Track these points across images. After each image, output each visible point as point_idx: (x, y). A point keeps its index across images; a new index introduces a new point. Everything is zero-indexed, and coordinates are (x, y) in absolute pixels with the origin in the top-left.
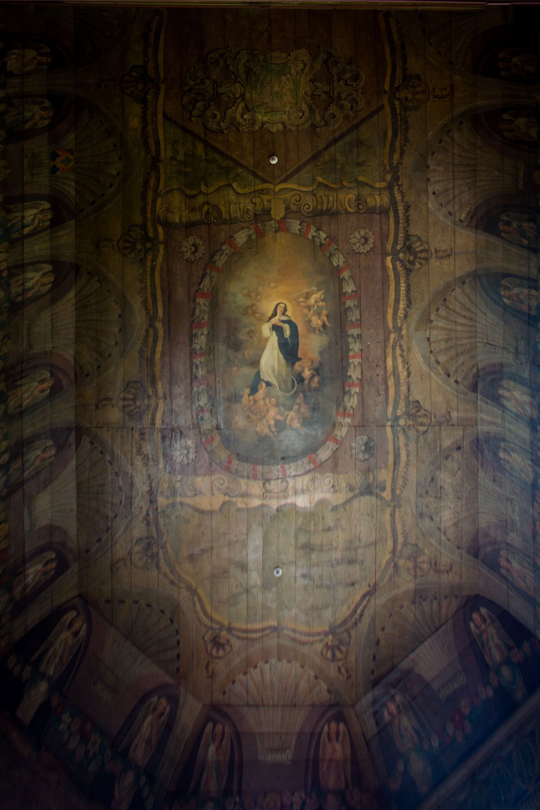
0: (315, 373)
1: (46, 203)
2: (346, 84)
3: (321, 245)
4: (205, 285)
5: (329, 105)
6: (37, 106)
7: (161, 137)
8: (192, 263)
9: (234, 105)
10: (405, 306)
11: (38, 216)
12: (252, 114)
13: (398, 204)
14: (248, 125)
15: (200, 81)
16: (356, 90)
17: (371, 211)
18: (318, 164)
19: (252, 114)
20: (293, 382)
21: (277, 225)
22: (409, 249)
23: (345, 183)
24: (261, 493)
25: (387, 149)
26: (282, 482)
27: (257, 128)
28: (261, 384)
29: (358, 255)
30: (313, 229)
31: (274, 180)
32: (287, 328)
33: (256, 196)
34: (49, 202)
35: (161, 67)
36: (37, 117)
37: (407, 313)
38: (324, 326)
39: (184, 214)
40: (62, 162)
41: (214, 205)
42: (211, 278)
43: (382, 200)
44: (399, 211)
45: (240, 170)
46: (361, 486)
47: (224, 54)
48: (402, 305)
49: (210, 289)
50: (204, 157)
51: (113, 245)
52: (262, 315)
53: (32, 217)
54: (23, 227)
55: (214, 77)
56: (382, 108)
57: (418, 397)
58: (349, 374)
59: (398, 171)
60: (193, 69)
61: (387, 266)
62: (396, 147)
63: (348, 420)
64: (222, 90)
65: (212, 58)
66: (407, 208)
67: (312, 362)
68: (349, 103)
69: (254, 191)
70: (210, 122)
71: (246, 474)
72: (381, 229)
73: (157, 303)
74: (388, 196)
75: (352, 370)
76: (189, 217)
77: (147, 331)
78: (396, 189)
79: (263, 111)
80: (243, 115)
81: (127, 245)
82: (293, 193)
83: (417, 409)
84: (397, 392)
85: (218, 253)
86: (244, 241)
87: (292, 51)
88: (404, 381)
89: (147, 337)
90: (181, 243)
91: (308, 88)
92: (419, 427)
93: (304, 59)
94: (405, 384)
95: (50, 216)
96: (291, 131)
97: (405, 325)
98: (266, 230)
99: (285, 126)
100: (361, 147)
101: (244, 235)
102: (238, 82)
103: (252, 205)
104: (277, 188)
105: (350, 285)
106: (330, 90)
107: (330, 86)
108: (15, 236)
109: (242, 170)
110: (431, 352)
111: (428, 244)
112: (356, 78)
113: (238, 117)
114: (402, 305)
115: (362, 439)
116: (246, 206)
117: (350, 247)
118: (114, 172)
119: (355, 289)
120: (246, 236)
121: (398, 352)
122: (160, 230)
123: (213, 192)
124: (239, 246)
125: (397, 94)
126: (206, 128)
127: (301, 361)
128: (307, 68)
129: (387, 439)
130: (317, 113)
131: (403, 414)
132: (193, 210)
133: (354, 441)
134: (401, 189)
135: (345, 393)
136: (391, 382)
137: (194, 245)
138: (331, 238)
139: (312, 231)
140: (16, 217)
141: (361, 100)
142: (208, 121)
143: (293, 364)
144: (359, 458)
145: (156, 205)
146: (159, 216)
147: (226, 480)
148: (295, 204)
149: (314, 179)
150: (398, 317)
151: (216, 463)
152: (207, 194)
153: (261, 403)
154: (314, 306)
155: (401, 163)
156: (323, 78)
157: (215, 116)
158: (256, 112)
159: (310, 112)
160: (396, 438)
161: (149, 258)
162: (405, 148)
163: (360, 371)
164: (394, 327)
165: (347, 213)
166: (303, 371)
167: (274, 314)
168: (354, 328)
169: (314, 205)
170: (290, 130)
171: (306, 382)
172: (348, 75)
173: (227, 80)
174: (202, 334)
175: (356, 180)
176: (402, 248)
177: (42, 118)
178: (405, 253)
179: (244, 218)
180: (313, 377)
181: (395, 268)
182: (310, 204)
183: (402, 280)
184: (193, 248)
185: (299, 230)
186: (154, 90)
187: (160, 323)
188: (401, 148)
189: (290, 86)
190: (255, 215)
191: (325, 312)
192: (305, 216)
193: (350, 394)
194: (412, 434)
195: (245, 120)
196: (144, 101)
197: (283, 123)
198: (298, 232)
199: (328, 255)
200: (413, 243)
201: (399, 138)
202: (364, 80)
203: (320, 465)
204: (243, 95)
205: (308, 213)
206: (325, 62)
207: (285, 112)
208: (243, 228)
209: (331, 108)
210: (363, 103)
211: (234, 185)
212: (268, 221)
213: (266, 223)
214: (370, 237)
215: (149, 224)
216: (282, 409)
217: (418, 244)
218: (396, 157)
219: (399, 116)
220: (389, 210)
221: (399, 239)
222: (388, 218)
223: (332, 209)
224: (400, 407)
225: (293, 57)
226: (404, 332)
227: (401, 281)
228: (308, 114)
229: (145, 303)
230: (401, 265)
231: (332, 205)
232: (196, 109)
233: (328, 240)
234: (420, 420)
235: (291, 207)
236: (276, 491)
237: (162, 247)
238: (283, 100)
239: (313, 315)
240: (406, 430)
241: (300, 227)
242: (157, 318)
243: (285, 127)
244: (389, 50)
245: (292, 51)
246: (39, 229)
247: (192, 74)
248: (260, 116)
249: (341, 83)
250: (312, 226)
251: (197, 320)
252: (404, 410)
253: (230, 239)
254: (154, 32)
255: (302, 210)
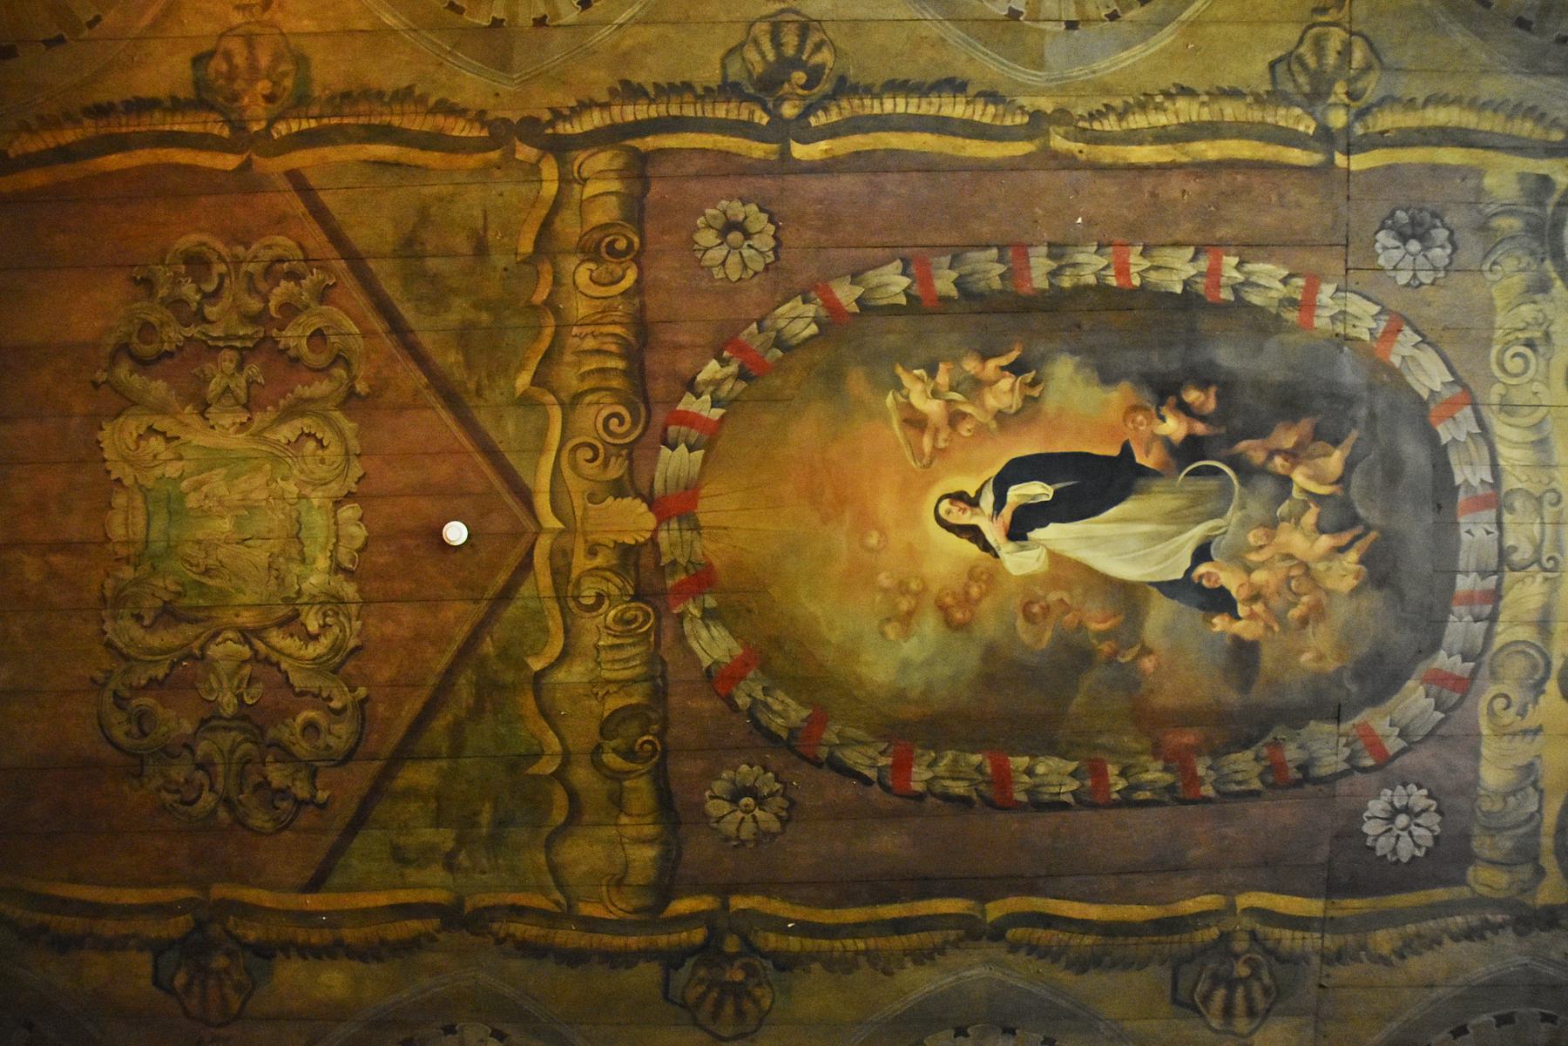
0: (1172, 400)
2: (216, 295)
3: (742, 375)
4: (869, 762)
7: (383, 899)
8: (793, 803)
9: (277, 664)
10: (961, 99)
12: (306, 604)
13: (618, 119)
14: (342, 618)
15: (200, 774)
16: (237, 262)
17: (635, 210)
18: (471, 386)
19: (306, 604)
20: (1196, 473)
21: (674, 525)
22: (768, 87)
23: (541, 296)
24: (1540, 577)
25: (433, 158)
26: (1512, 510)
27: (350, 590)
28: (1201, 577)
29: (783, 255)
30: (688, 404)
31: (522, 534)
32: (1019, 493)
33: (576, 593)
35: (158, 895)
37: (980, 94)
38: (1016, 368)
39: (631, 832)
41: (602, 733)
42: (846, 742)
43: (600, 175)
44: (639, 117)
45: (488, 647)
46: (1532, 253)
47: (115, 693)
48: (956, 109)
49: (883, 746)
50: (444, 764)
52: (972, 575)
55: (187, 727)
56: (296, 179)
57: (1261, 67)
58: (1178, 289)
59: (505, 121)
60: (164, 794)
61: (824, 156)
62: (425, 128)
63: (1326, 292)
64: (228, 702)
65: (128, 734)
66: (631, 92)
67: (1135, 409)
69: (558, 599)
70: (332, 741)
71: (1481, 627)
72: (698, 176)
73: (920, 916)
74: (589, 152)
75: (1168, 277)
76: (644, 816)
77: (1014, 948)
78: (568, 126)
79: (296, 568)
80: (308, 632)
81: (729, 1009)
82: (567, 472)
83: (1296, 67)
84: (1242, 131)
85: (764, 718)
86: (725, 633)
87: (109, 472)
88: (1206, 109)
89: (1033, 949)
90: (727, 839)
91: (227, 420)
92: (1354, 65)
93: (135, 435)
94: (1216, 107)
97: (1023, 101)
98: (689, 561)
99: (345, 496)
100: (422, 244)
101: (704, 633)
102: (203, 648)
103: (604, 607)
104: (551, 522)
105: (885, 279)
106: (232, 348)
107: (220, 349)
109: (488, 639)
110: (1113, 17)
111: (752, 24)
112: (197, 263)
113: (313, 650)
114: (956, 109)
115: (1385, 248)
116: (607, 627)
117: (756, 280)
119: (898, 264)
120: (707, 627)
121: (1110, 124)
122: (683, 906)
123: (557, 734)
124: (739, 651)
125: (255, 128)
126: (349, 756)
127: (1134, 446)
128: (162, 423)
129: (1389, 167)
130: (307, 392)
131: (1311, 114)
132: (617, 802)
133: (1392, 274)
134: (566, 112)
135: (1241, 304)
136: (1209, 150)
137: (734, 798)
138: (723, 345)
139: (700, 406)
141: (270, 247)
142: (328, 747)
143: (1143, 472)
144: (1447, 261)
145: (605, 920)
146: (636, 911)
147: (1493, 689)
148: (606, 464)
150: (998, 123)
151: (1442, 722)
152: (567, 758)
153: (1259, 577)
154: (949, 402)
155: (482, 113)
156: (196, 371)
157: (311, 726)
158: (299, 593)
159: (303, 414)
160: (1380, 141)
161: (772, 941)
162: (432, 100)
163: (1168, 251)
164: (1029, 138)
165: (639, 288)
166: (1166, 440)
167: (973, 533)
168: (1029, 268)
169: (608, 400)
171: (1200, 428)
172: (188, 290)
173: (198, 685)
174: (1030, 772)
175: (530, 260)
176: (765, 109)
178: (781, 100)
180: (1185, 409)
181: (831, 132)
182: (605, 413)
183: (873, 107)
184: (745, 800)
185: (691, 449)
186: (231, 917)
187: (990, 906)
188: (432, 111)
189: (217, 482)
191: (971, 365)
192: (645, 429)
193: (1242, 284)
194: (1372, 86)
195: (324, 626)
196: (265, 952)
197: (338, 503)
198: (699, 454)
199: (779, 353)
200: (750, 73)
201: (396, 121)
202: (205, 238)
203: (1465, 387)
204: (246, 635)
205: (635, 424)
206: (143, 364)
207: (301, 497)
208: (681, 638)
209: (292, 343)
210: (280, 239)
211: (536, 665)
212: (658, 554)
213: (665, 560)
214: (725, 213)
215: (663, 940)
216: (1283, 509)
217: (752, 55)
218: (460, 129)
219: (325, 121)
220: (636, 150)
221: (733, 116)
222: (662, 151)
223: (623, 338)
224: (1291, 124)
225: (128, 470)
226: (1047, 105)
227: (877, 111)
228: (307, 421)
229: (922, 957)
230: (820, 113)
231: (610, 339)
232: (289, 787)
233: (726, 354)
234: (1331, 59)
235: (616, 476)
236: (1536, 528)
237: (739, 903)
239: (983, 406)
240: (1360, 104)
241: (682, 448)
242: (972, 917)
243: (350, 496)
244: (113, 157)
245: (109, 472)
247: (177, 797)
248: (313, 580)
249: (211, 311)
250: (680, 407)
251: (982, 787)
252: (1298, 111)
253: (719, 680)
254: (48, 917)
255: (627, 440)
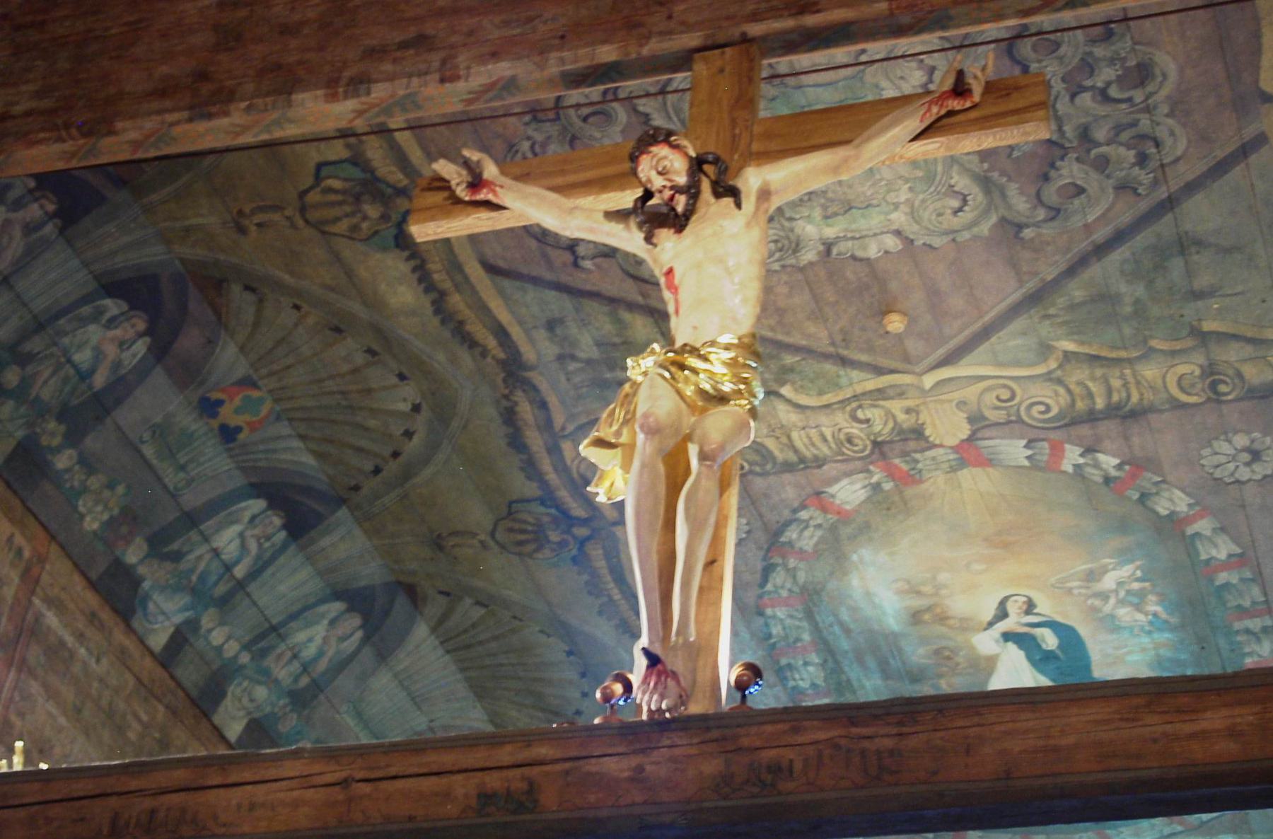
1: (251, 502)
2: (1103, 95)
5: (1052, 165)
6: (92, 328)
11: (248, 533)
16: (1148, 110)
18: (1052, 311)
23: (1154, 343)
34: (258, 497)
36: (111, 351)
40: (237, 411)
51: (482, 542)
53: (237, 543)
54: (228, 568)
68: (1129, 147)
95: (277, 521)
96: (935, 249)
100: (1198, 253)
108: (221, 589)
109: (798, 358)
118: (405, 407)
119: (1238, 551)
140: (200, 558)
141: (1172, 134)
149: (1045, 350)
158: (791, 219)
170: (930, 246)
172: (1106, 74)
177: (123, 345)
179: (843, 454)
190: (876, 444)
197: (898, 233)
211: (786, 391)
223: (1125, 406)
228: (980, 197)
233: (1127, 467)
238: (878, 177)
246: (268, 554)
249: (1086, 99)
